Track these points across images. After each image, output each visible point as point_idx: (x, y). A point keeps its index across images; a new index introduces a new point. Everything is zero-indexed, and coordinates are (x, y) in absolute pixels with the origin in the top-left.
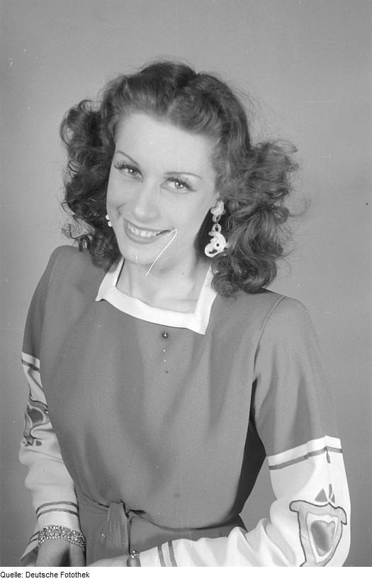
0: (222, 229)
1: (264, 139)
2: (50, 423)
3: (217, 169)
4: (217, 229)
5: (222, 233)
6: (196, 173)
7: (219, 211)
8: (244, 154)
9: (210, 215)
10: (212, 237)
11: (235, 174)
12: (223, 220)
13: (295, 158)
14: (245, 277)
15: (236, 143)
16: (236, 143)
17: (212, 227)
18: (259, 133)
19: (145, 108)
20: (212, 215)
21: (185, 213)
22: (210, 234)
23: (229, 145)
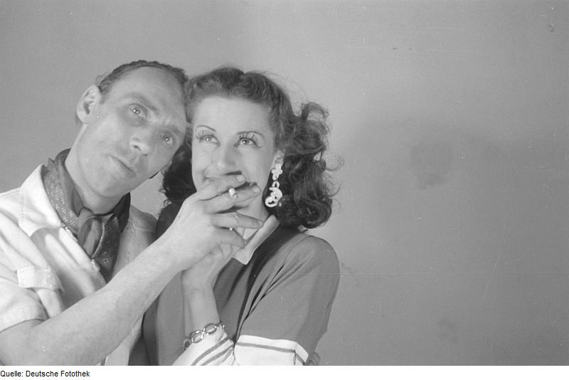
5: (279, 188)
22: (271, 189)
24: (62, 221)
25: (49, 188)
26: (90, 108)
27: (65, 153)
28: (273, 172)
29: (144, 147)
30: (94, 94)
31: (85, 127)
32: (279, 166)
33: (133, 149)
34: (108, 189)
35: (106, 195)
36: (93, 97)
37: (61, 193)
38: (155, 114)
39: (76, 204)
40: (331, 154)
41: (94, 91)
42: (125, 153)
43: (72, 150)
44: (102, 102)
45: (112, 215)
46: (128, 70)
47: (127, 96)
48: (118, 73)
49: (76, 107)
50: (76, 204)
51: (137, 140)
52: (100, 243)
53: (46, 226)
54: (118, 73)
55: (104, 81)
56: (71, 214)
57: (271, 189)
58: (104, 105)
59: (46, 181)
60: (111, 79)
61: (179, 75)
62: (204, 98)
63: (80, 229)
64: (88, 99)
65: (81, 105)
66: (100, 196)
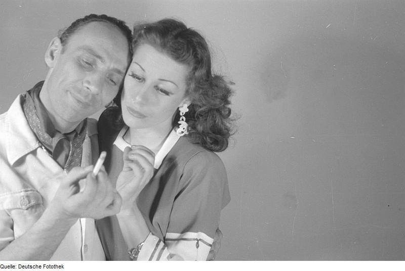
0: (186, 120)
1: (218, 73)
2: (82, 219)
3: (188, 84)
4: (183, 120)
5: (186, 121)
6: (172, 79)
7: (184, 109)
8: (204, 79)
9: (178, 112)
10: (180, 124)
11: (196, 90)
12: (186, 115)
13: (231, 87)
14: (77, 133)
15: (200, 73)
16: (200, 73)
17: (179, 119)
18: (217, 68)
19: (153, 44)
20: (180, 111)
21: (164, 106)
22: (179, 123)
23: (223, 112)
24: (40, 142)
25: (28, 115)
26: (54, 55)
27: (40, 84)
28: (180, 109)
29: (93, 89)
30: (57, 44)
31: (51, 71)
32: (186, 106)
33: (86, 89)
34: (71, 118)
35: (71, 121)
36: (56, 47)
37: (39, 122)
38: (102, 62)
39: (51, 128)
40: (216, 97)
41: (57, 42)
42: (80, 91)
43: (45, 83)
44: (63, 51)
45: (75, 134)
46: (82, 25)
47: (79, 48)
48: (75, 26)
49: (45, 54)
50: (51, 128)
51: (89, 83)
52: (70, 156)
53: (42, 192)
54: (75, 26)
55: (64, 34)
56: (47, 136)
57: (179, 123)
58: (64, 55)
59: (25, 109)
60: (68, 33)
61: (121, 25)
62: (146, 43)
63: (124, 169)
64: (53, 48)
65: (48, 54)
66: (66, 121)
